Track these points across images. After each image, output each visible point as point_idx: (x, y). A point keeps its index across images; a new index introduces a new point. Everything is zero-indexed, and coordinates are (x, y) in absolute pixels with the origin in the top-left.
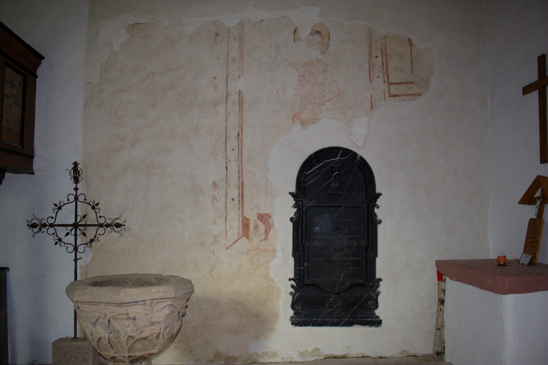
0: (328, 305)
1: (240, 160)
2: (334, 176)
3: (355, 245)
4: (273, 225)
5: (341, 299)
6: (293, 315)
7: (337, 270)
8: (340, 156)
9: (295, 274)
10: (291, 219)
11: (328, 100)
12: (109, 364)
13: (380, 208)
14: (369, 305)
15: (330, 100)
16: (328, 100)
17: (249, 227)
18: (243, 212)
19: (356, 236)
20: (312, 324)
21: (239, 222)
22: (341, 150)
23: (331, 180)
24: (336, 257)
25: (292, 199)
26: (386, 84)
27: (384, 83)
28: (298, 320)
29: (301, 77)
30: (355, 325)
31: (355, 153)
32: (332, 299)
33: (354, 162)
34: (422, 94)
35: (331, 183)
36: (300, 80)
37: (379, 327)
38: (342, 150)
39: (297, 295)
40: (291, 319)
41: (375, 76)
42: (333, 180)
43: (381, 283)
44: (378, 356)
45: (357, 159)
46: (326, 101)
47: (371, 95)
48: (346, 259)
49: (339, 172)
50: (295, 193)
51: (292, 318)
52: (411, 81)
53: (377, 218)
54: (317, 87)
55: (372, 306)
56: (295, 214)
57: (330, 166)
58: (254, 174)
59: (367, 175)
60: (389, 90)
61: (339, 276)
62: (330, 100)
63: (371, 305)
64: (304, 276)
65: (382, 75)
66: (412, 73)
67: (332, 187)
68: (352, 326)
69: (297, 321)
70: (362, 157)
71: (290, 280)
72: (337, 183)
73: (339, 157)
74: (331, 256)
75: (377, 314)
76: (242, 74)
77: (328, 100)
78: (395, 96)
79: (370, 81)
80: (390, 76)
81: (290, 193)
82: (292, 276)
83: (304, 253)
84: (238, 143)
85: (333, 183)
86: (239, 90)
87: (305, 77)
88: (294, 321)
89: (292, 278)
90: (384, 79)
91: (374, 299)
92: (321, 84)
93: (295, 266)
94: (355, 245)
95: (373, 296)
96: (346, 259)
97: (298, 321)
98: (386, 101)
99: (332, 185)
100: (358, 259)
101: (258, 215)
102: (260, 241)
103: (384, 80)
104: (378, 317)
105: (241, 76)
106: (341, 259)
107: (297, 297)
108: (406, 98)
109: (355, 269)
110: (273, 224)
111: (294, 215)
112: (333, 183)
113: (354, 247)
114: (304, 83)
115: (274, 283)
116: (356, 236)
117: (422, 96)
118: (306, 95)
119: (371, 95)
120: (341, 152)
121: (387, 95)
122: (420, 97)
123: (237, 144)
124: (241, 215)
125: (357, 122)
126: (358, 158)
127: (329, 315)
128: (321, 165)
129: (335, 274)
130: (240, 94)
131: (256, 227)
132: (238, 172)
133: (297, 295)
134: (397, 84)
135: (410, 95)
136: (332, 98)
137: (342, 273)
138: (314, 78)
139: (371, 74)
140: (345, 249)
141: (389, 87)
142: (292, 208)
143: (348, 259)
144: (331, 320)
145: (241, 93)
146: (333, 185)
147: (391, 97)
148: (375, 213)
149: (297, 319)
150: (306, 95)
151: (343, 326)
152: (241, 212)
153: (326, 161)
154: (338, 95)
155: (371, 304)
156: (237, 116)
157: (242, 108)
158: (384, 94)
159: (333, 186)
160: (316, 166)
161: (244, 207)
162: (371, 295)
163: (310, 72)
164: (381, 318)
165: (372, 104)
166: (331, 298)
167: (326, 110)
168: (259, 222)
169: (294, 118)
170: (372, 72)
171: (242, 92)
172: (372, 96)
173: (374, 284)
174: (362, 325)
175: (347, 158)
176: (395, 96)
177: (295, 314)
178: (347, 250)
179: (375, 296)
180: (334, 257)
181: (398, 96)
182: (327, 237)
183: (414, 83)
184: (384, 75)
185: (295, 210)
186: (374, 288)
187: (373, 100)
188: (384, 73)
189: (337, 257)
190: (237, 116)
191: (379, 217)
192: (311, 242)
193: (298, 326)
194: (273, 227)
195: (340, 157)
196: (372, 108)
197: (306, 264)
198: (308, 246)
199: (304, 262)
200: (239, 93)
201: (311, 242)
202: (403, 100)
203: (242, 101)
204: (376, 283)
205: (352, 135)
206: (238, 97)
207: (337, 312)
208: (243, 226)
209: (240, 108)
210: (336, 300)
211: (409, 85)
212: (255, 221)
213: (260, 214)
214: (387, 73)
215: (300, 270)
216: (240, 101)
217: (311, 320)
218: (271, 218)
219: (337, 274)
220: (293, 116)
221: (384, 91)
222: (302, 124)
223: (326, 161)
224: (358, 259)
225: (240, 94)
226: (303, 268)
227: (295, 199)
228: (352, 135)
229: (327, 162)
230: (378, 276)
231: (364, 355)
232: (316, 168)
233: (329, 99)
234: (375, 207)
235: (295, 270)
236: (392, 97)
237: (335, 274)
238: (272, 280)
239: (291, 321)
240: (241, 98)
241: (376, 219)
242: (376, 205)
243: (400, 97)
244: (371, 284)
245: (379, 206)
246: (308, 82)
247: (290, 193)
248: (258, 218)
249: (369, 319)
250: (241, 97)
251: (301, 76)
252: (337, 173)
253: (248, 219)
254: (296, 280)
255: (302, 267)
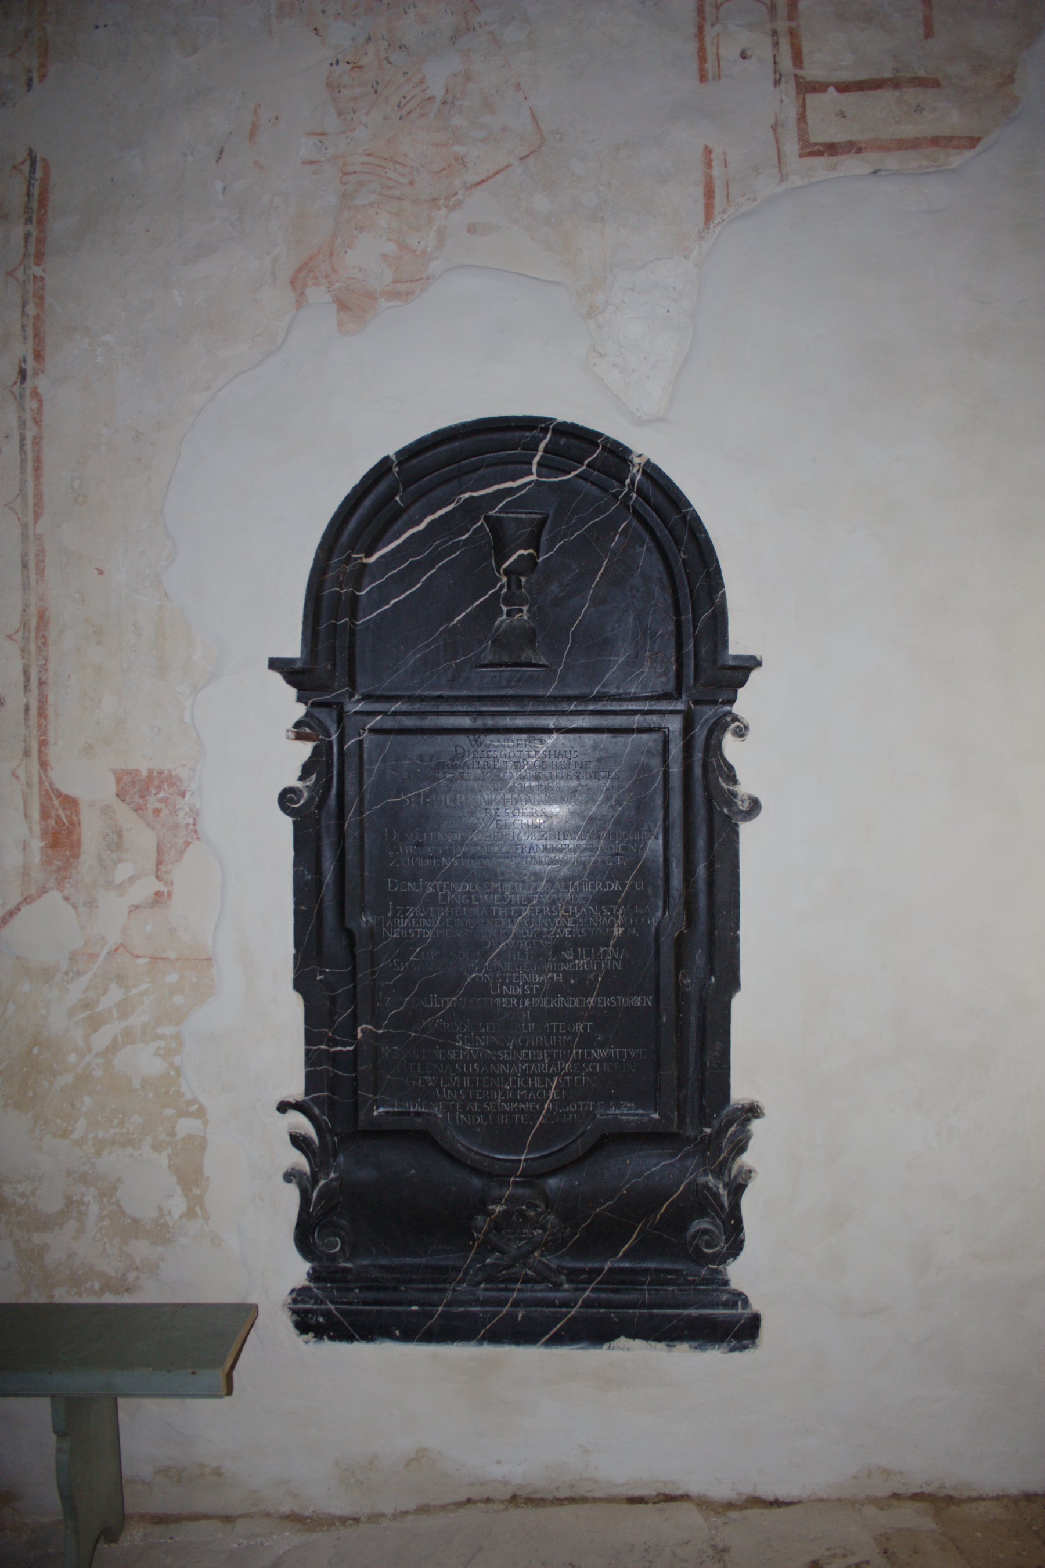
0: (481, 1236)
1: (31, 501)
2: (507, 572)
3: (618, 931)
4: (196, 831)
5: (547, 1207)
6: (307, 1283)
7: (523, 1062)
8: (539, 464)
9: (312, 1081)
10: (286, 799)
11: (478, 179)
12: (14, 1405)
13: (751, 736)
14: (694, 1237)
15: (488, 178)
16: (480, 183)
17: (79, 844)
18: (44, 765)
19: (623, 886)
20: (397, 1332)
21: (26, 815)
22: (545, 430)
23: (493, 591)
24: (519, 991)
25: (292, 692)
26: (789, 87)
27: (777, 83)
28: (329, 1311)
29: (338, 70)
30: (623, 1341)
31: (619, 445)
32: (498, 1208)
33: (615, 496)
34: (979, 139)
35: (491, 609)
36: (333, 86)
37: (744, 1348)
38: (549, 435)
39: (322, 1182)
40: (295, 1301)
41: (730, 51)
42: (505, 590)
43: (756, 1126)
44: (739, 1494)
45: (628, 481)
46: (470, 188)
47: (706, 147)
48: (572, 1003)
49: (537, 550)
50: (299, 665)
51: (300, 1294)
52: (922, 73)
53: (735, 789)
54: (422, 116)
55: (709, 1245)
56: (307, 770)
57: (487, 519)
58: (101, 572)
59: (683, 560)
60: (802, 118)
61: (535, 1090)
62: (488, 178)
63: (707, 1237)
64: (355, 1089)
65: (768, 41)
66: (928, 35)
67: (499, 627)
68: (606, 1346)
69: (324, 1316)
70: (656, 468)
71: (283, 1107)
72: (525, 608)
73: (534, 469)
74: (495, 990)
75: (735, 1284)
76: (43, 65)
77: (480, 183)
78: (832, 149)
79: (703, 78)
80: (806, 47)
81: (275, 664)
82: (296, 1089)
83: (354, 973)
84: (20, 417)
85: (505, 609)
86: (31, 150)
87: (360, 67)
88: (307, 1312)
89: (291, 1100)
90: (775, 63)
91: (722, 1206)
92: (444, 103)
93: (310, 1038)
94: (621, 930)
95: (716, 1195)
96: (572, 1003)
97: (327, 1313)
98: (783, 178)
99: (500, 619)
100: (636, 1001)
101: (118, 781)
102: (130, 912)
103: (775, 71)
104: (740, 1298)
105: (35, 80)
106: (544, 1004)
107: (321, 1195)
108: (891, 161)
109: (622, 1054)
110: (194, 825)
111: (301, 778)
112: (505, 609)
113: (612, 943)
114: (355, 99)
115: (206, 1123)
116: (623, 886)
117: (978, 149)
118: (367, 159)
119: (706, 147)
120: (542, 446)
121: (791, 146)
122: (968, 154)
123: (15, 424)
124: (36, 780)
125: (632, 289)
126: (635, 471)
127: (489, 1286)
128: (442, 516)
129: (515, 1082)
130: (33, 170)
131: (116, 842)
132: (20, 565)
133: (325, 1185)
134: (844, 88)
135: (913, 144)
136: (497, 173)
137: (551, 1077)
138: (405, 73)
139: (708, 39)
140: (567, 955)
141: (804, 106)
142: (288, 738)
143: (581, 1002)
144: (495, 1314)
145: (38, 165)
146: (504, 616)
147: (812, 154)
148: (730, 1002)
149: (322, 1302)
150: (367, 159)
151: (557, 1340)
152: (35, 765)
153: (467, 495)
154: (532, 153)
155: (706, 1232)
156: (16, 279)
157: (40, 241)
158: (777, 141)
159: (502, 622)
160: (418, 524)
161: (51, 739)
162: (706, 1186)
163: (386, 44)
164: (756, 1305)
165: (709, 194)
166: (497, 1201)
167: (469, 231)
168: (124, 814)
169: (298, 283)
170: (710, 32)
171: (44, 160)
172: (708, 151)
173: (721, 1131)
174: (659, 1340)
175: (577, 476)
176: (832, 149)
177: (314, 1276)
178: (576, 957)
179: (723, 1191)
180: (507, 995)
181: (849, 152)
182: (468, 887)
183: (936, 84)
184: (776, 44)
185: (305, 750)
186: (720, 1150)
187: (717, 171)
188: (775, 33)
189: (524, 996)
190: (16, 279)
191: (746, 786)
192: (390, 914)
193: (332, 1338)
194: (198, 838)
195: (538, 475)
196: (709, 216)
197: (362, 1030)
198: (373, 934)
199: (354, 1020)
200: (26, 167)
201: (390, 914)
202: (875, 172)
203: (43, 202)
204: (729, 1124)
205: (601, 355)
206: (24, 187)
207: (530, 1273)
208: (44, 833)
209: (33, 240)
210: (522, 1214)
211: (911, 95)
212: (107, 810)
213: (133, 774)
214: (793, 34)
215: (335, 1059)
216: (35, 205)
217: (398, 1308)
218: (183, 795)
219: (526, 1082)
220: (300, 270)
221: (774, 128)
222: (342, 306)
223: (467, 495)
224: (636, 1001)
225: (33, 170)
226: (351, 1048)
227: (307, 693)
228: (601, 355)
229: (471, 498)
230: (739, 1093)
231: (667, 1490)
232: (418, 533)
233: (483, 177)
234: (725, 729)
235: (312, 1059)
236: (820, 153)
237: (515, 1082)
238: (194, 1108)
239: (294, 1312)
240: (36, 192)
241: (734, 795)
242: (729, 719)
243: (863, 155)
244: (708, 1130)
245: (746, 728)
246: (376, 92)
247: (275, 664)
248: (118, 795)
249: (694, 1312)
250: (37, 184)
251: (337, 62)
252: (522, 556)
253: (71, 802)
254: (317, 1111)
255: (345, 1045)
